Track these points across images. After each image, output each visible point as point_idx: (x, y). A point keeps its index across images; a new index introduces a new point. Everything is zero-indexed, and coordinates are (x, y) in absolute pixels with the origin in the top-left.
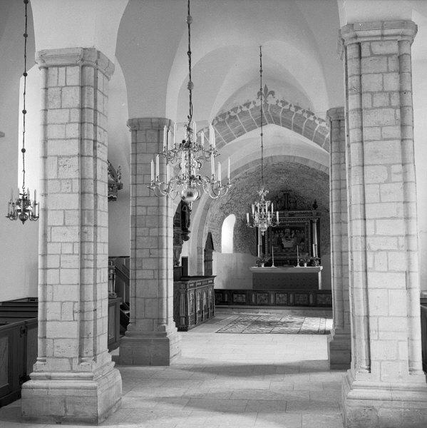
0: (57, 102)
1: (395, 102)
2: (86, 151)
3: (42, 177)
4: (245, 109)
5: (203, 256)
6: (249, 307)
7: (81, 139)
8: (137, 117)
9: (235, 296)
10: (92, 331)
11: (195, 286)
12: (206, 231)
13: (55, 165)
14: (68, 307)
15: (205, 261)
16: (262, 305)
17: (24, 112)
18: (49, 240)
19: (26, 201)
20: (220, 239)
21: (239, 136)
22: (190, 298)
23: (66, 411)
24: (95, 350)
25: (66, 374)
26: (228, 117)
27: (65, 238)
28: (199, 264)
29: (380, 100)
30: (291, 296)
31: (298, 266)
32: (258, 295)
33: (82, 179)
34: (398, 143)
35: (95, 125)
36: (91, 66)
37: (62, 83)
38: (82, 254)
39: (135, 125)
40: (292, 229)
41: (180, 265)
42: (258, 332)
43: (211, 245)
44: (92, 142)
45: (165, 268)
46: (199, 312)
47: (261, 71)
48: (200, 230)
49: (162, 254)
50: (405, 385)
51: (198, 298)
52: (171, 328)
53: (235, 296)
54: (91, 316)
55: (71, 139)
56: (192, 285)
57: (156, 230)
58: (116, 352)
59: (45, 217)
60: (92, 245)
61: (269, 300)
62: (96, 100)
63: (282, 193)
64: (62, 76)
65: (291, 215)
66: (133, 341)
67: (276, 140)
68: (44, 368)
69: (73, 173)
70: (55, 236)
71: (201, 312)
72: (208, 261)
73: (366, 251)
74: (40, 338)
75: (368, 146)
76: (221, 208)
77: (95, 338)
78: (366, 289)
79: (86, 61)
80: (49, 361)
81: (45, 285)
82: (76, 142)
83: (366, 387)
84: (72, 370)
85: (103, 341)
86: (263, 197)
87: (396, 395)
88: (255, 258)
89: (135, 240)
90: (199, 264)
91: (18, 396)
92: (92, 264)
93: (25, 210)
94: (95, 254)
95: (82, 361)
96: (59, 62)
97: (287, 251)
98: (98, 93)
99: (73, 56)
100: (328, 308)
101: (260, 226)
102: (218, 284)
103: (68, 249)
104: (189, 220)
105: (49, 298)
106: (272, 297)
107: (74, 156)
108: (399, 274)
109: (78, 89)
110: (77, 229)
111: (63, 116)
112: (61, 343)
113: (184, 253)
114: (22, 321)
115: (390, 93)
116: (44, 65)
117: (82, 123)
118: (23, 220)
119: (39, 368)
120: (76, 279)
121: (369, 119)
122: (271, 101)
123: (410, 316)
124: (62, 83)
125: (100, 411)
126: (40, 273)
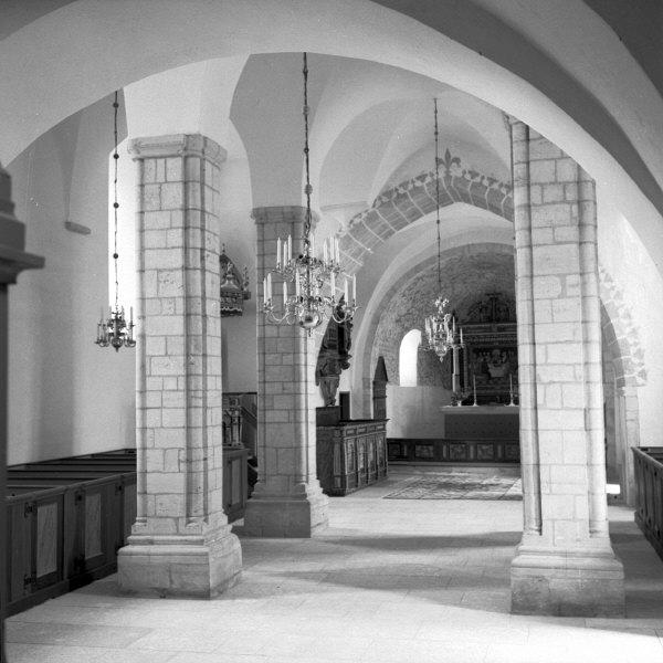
0: (155, 202)
1: (571, 195)
2: (191, 262)
3: (138, 227)
4: (418, 184)
5: (371, 390)
6: (439, 464)
7: (186, 248)
8: (264, 205)
9: (418, 448)
10: (202, 485)
11: (355, 434)
12: (376, 352)
13: (155, 283)
14: (172, 456)
15: (374, 398)
16: (457, 461)
17: (116, 205)
18: (148, 373)
19: (119, 322)
20: (398, 366)
21: (414, 220)
22: (348, 450)
23: (171, 582)
24: (205, 509)
25: (170, 538)
26: (395, 195)
27: (168, 370)
28: (366, 403)
29: (553, 193)
30: (499, 448)
31: (512, 405)
32: (451, 446)
33: (188, 298)
34: (575, 246)
35: (203, 230)
36: (196, 156)
37: (161, 179)
38: (188, 390)
39: (262, 217)
40: (502, 350)
41: (337, 403)
42: (444, 498)
43: (383, 375)
44: (199, 251)
45: (303, 407)
46: (363, 470)
47: (436, 133)
48: (367, 354)
49: (299, 389)
50: (584, 550)
51: (361, 450)
52: (313, 488)
53: (418, 448)
54: (201, 466)
55: (173, 248)
56: (351, 432)
57: (291, 356)
58: (240, 522)
59: (143, 344)
60: (201, 379)
61: (468, 455)
62: (203, 199)
63: (488, 298)
64: (161, 170)
65: (500, 330)
66: (262, 504)
67: (462, 221)
68: (145, 530)
69: (176, 290)
70: (156, 368)
71: (365, 470)
72: (380, 398)
73: (535, 384)
74: (140, 493)
75: (537, 252)
76: (397, 321)
77: (205, 494)
78: (536, 431)
79: (193, 151)
80: (151, 521)
81: (144, 429)
82: (180, 252)
83: (535, 552)
84: (178, 533)
85: (216, 499)
86: (440, 308)
87: (570, 562)
88: (448, 393)
89: (263, 370)
90: (366, 403)
91: (113, 568)
92: (200, 402)
93: (119, 334)
94: (205, 390)
95: (190, 522)
96: (157, 154)
97: (496, 383)
98: (207, 190)
99: (174, 145)
100: (515, 465)
101: (437, 349)
102: (393, 431)
103: (171, 384)
104: (349, 339)
105: (149, 445)
106: (472, 448)
107: (177, 269)
108: (575, 412)
109: (181, 186)
110: (182, 359)
111: (162, 220)
112: (164, 499)
113: (344, 386)
114: (119, 475)
115: (565, 185)
116: (139, 156)
117: (186, 228)
118: (117, 347)
119: (139, 530)
120: (182, 422)
121: (538, 218)
122: (456, 172)
123: (590, 465)
124: (161, 179)
125: (212, 582)
126: (138, 413)
